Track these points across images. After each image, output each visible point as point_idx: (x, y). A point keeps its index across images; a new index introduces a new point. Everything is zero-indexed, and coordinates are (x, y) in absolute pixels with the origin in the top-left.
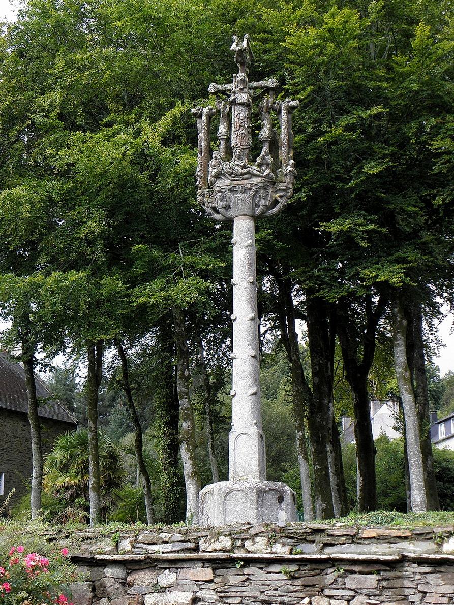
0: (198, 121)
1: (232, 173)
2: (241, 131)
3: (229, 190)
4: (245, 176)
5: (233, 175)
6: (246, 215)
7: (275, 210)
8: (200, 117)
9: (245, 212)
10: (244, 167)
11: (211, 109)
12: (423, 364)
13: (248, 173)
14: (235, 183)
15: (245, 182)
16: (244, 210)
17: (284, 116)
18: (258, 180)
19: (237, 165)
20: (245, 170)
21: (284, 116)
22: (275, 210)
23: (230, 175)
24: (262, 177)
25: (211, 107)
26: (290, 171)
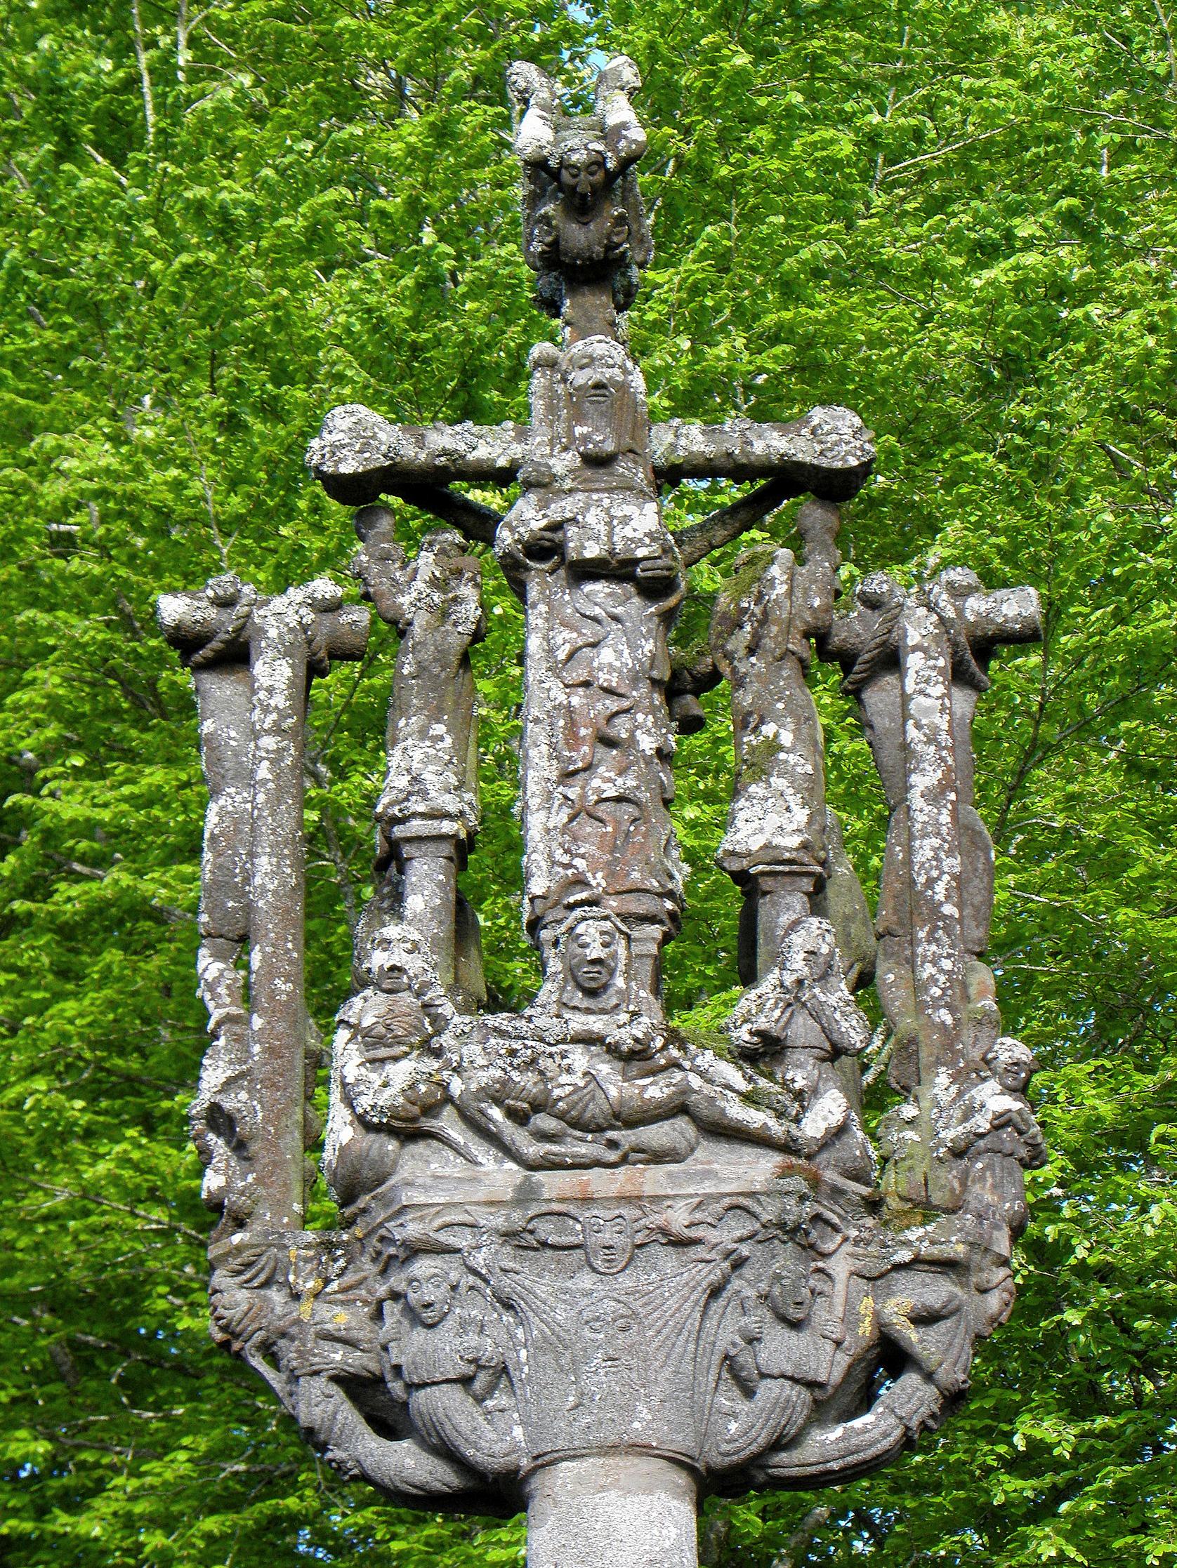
0: (220, 689)
1: (538, 1107)
2: (607, 781)
3: (509, 1235)
4: (657, 1135)
5: (543, 1122)
6: (640, 1449)
7: (874, 1428)
8: (235, 656)
9: (643, 1422)
10: (634, 1057)
11: (330, 607)
12: (458, 525)
13: (679, 1108)
14: (553, 1183)
15: (654, 1179)
16: (628, 1411)
17: (926, 697)
18: (759, 1168)
19: (587, 1040)
20: (656, 1090)
21: (926, 697)
22: (874, 1428)
23: (519, 1118)
24: (787, 1147)
25: (324, 586)
26: (1002, 1122)
